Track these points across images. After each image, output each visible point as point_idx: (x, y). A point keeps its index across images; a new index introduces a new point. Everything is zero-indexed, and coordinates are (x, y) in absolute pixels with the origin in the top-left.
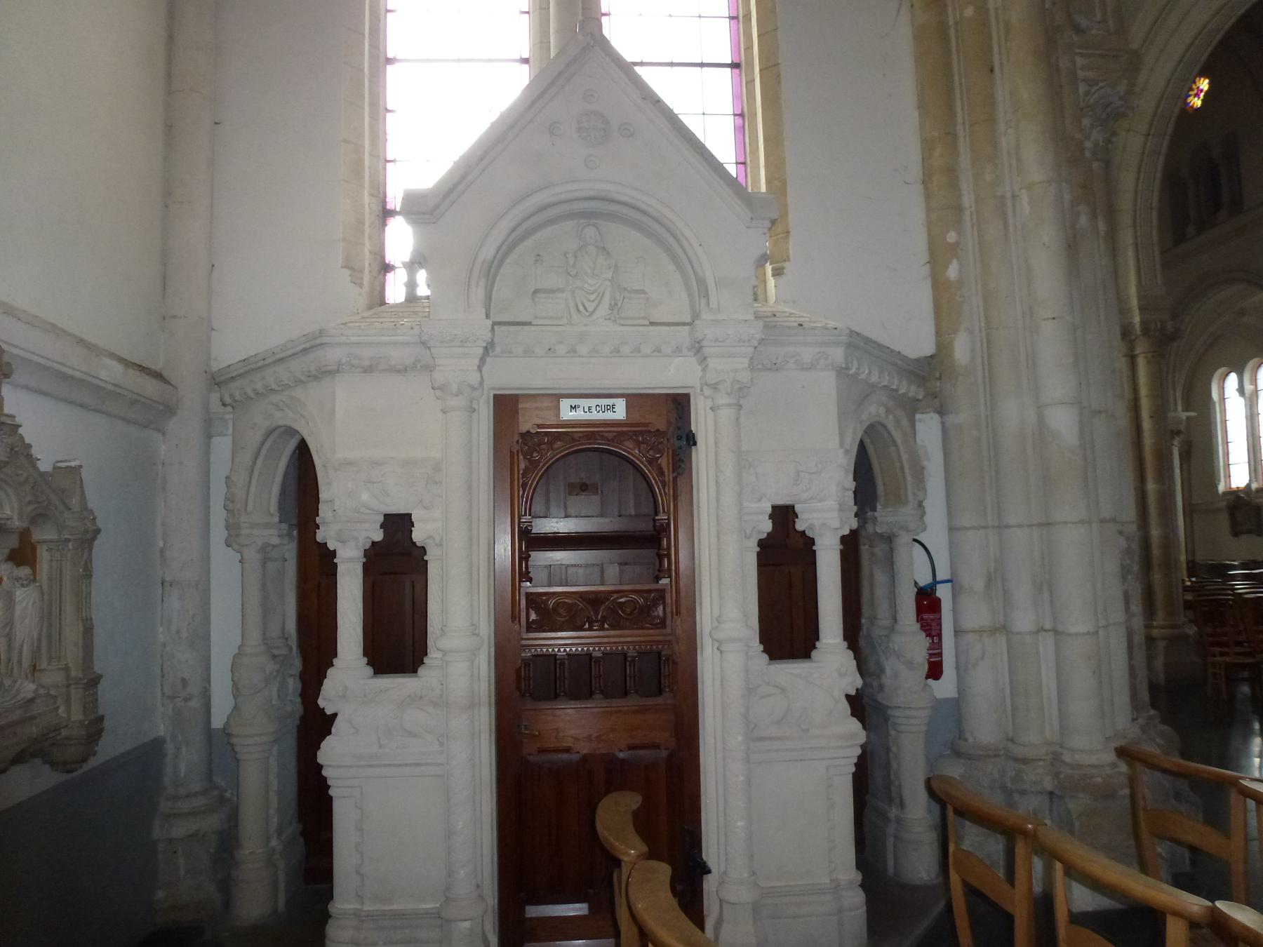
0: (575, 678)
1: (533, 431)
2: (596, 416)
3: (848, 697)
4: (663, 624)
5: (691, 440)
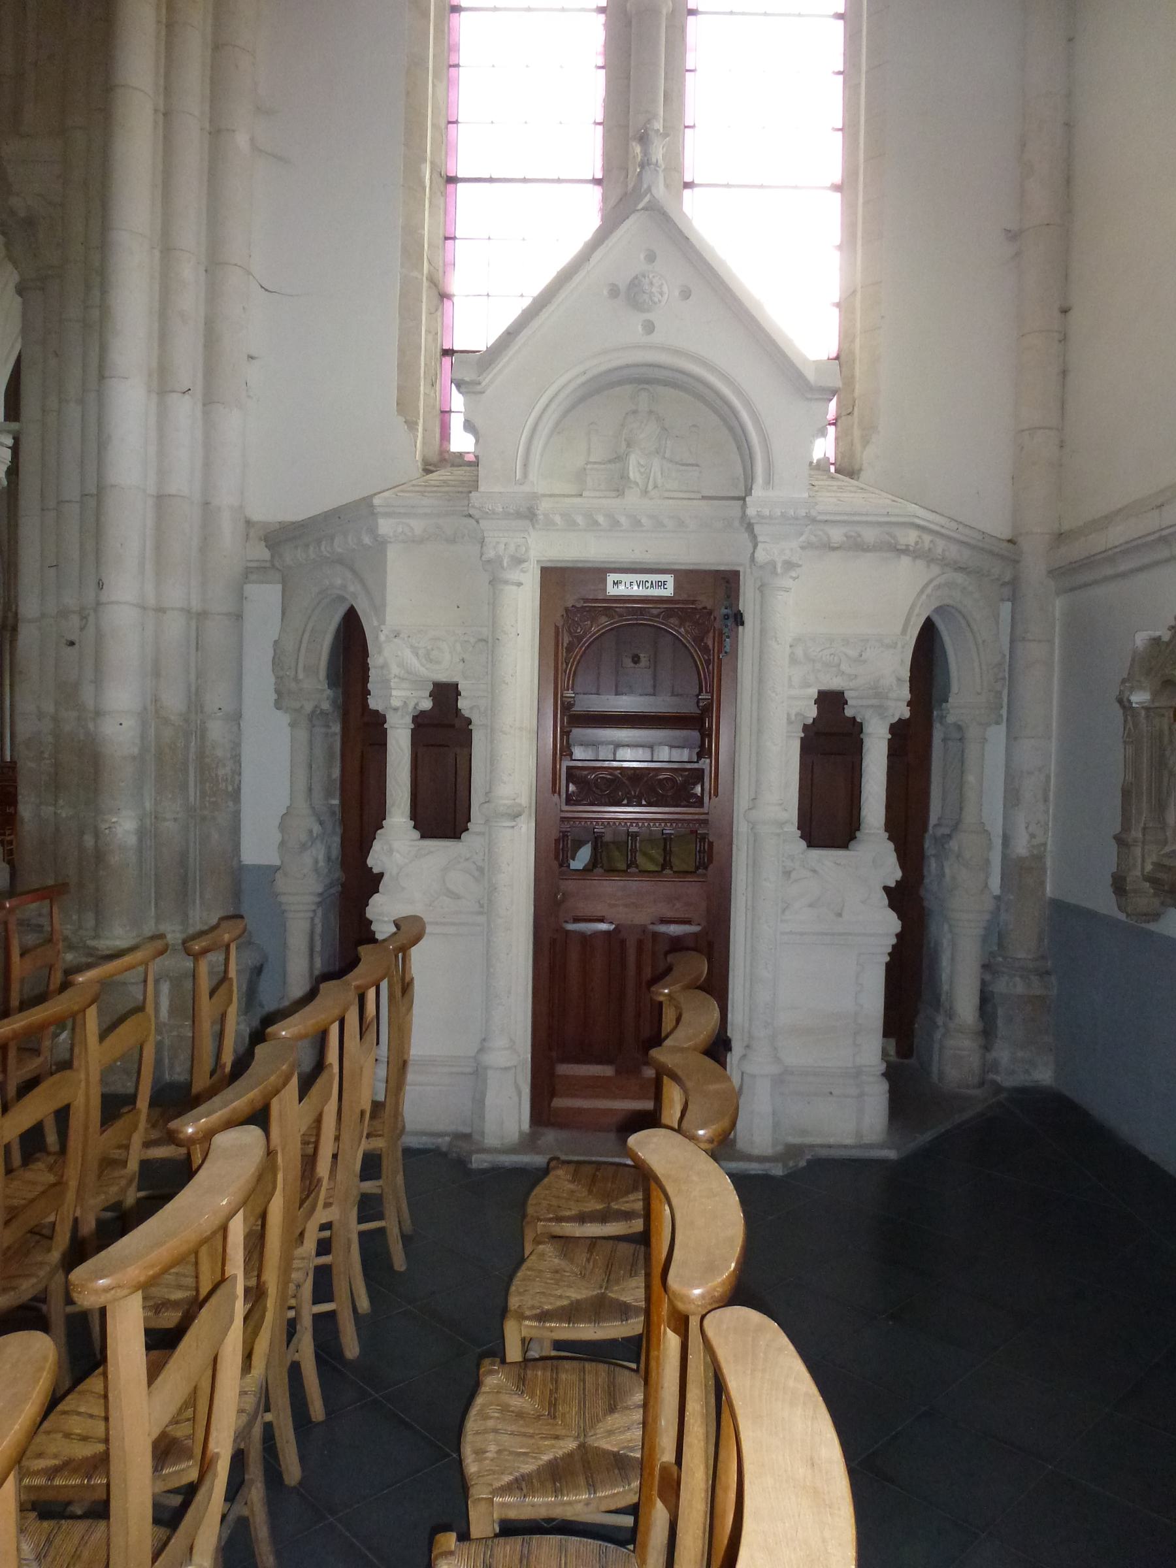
0: (614, 855)
1: (578, 605)
2: (636, 591)
3: (886, 889)
4: (700, 802)
5: (739, 619)
